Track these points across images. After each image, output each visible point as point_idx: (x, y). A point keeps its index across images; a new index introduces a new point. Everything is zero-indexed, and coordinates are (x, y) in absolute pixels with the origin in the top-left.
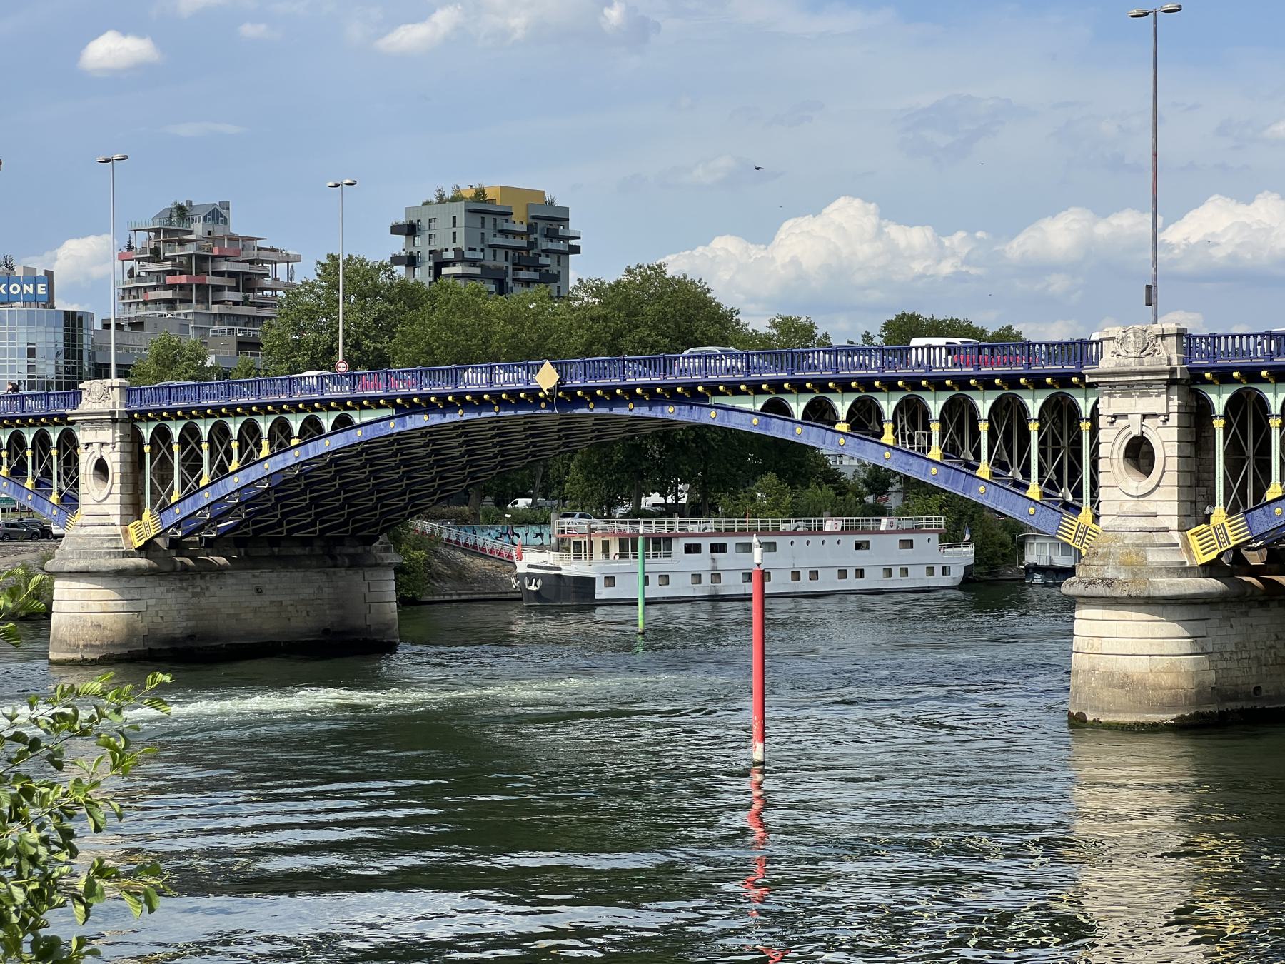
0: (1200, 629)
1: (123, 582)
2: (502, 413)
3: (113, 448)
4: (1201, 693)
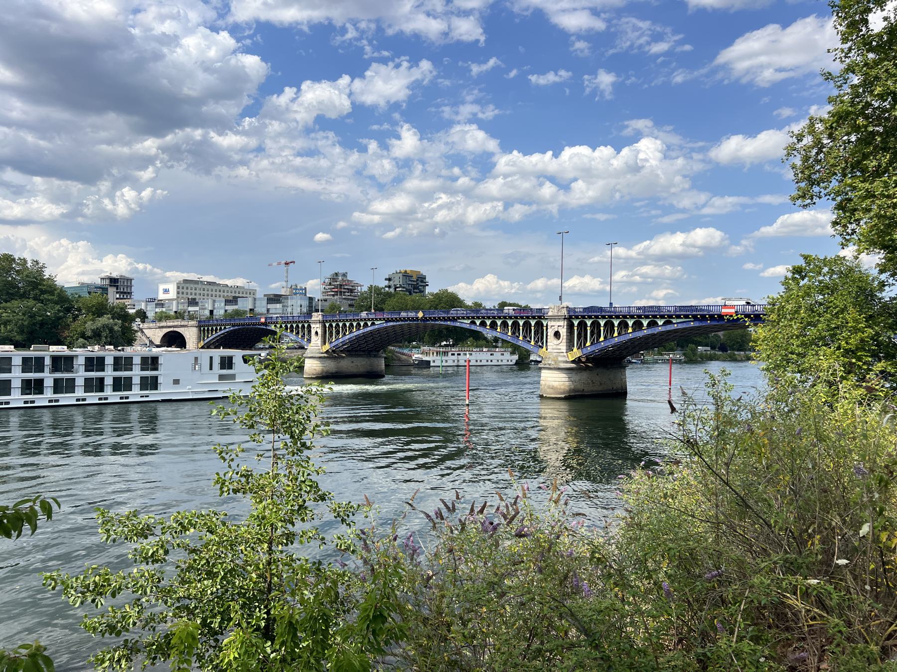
0: (570, 376)
4: (570, 391)
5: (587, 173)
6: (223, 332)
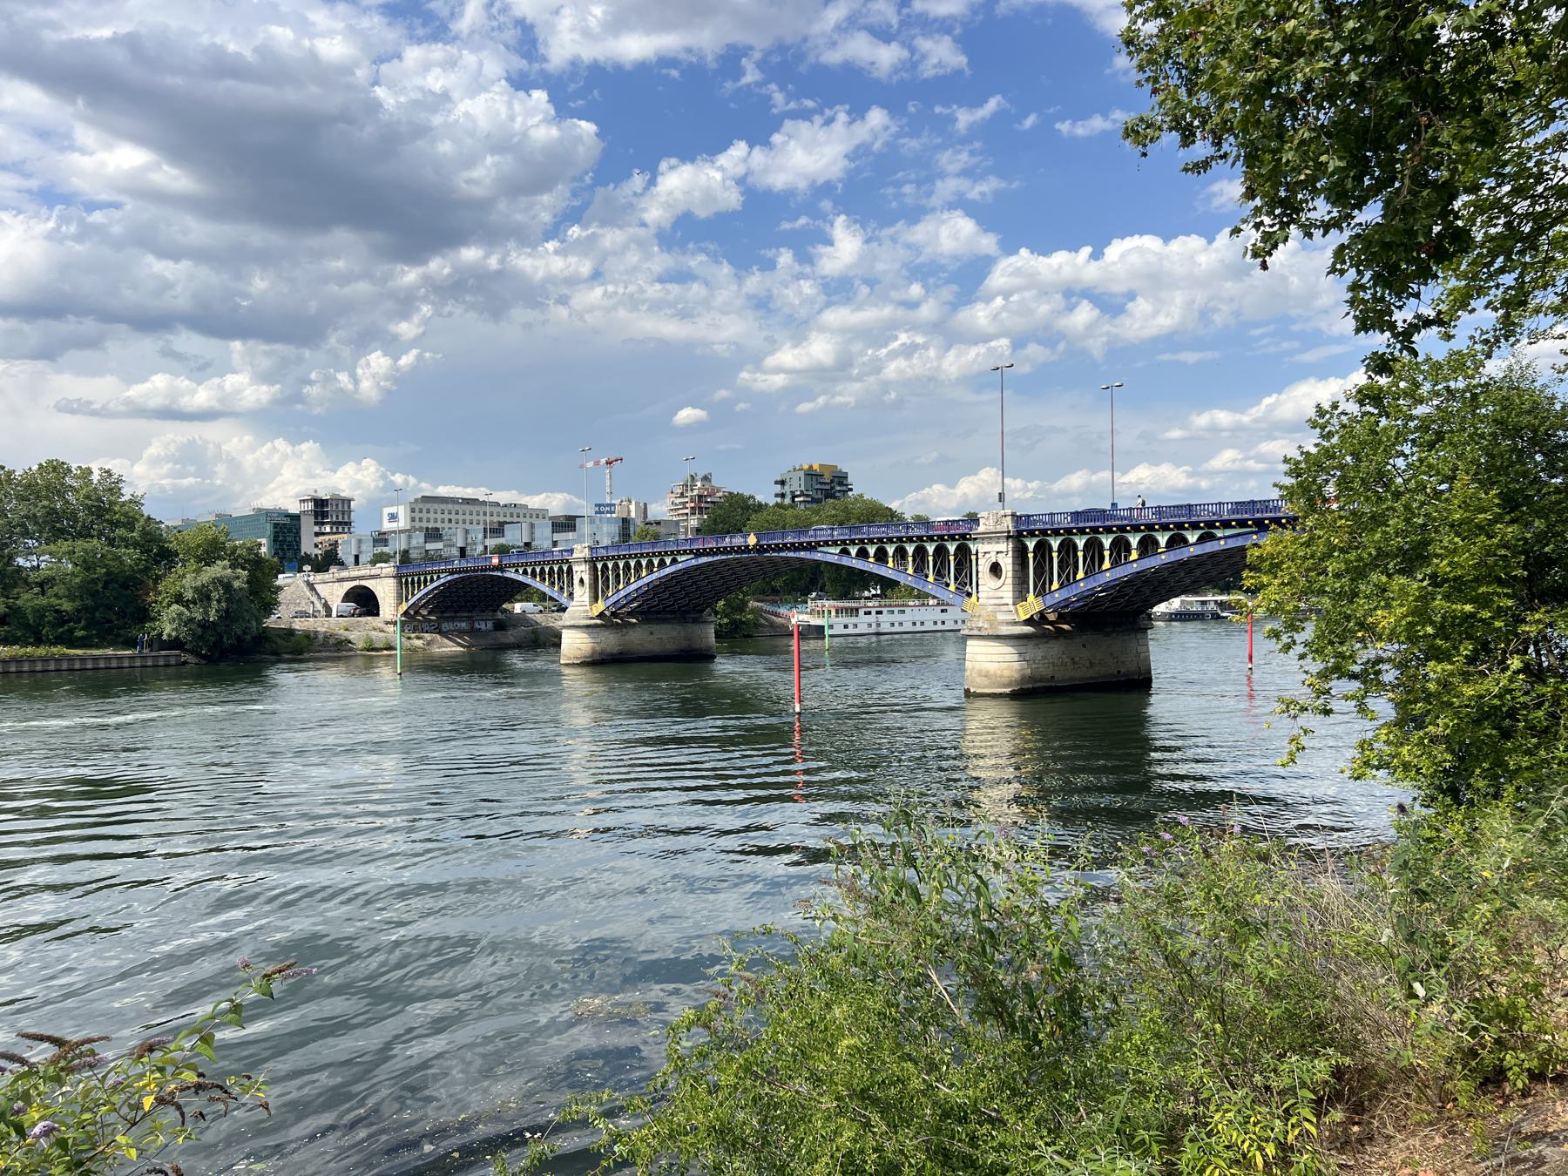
0: (1023, 649)
4: (1023, 679)
5: (1156, 281)
6: (435, 584)
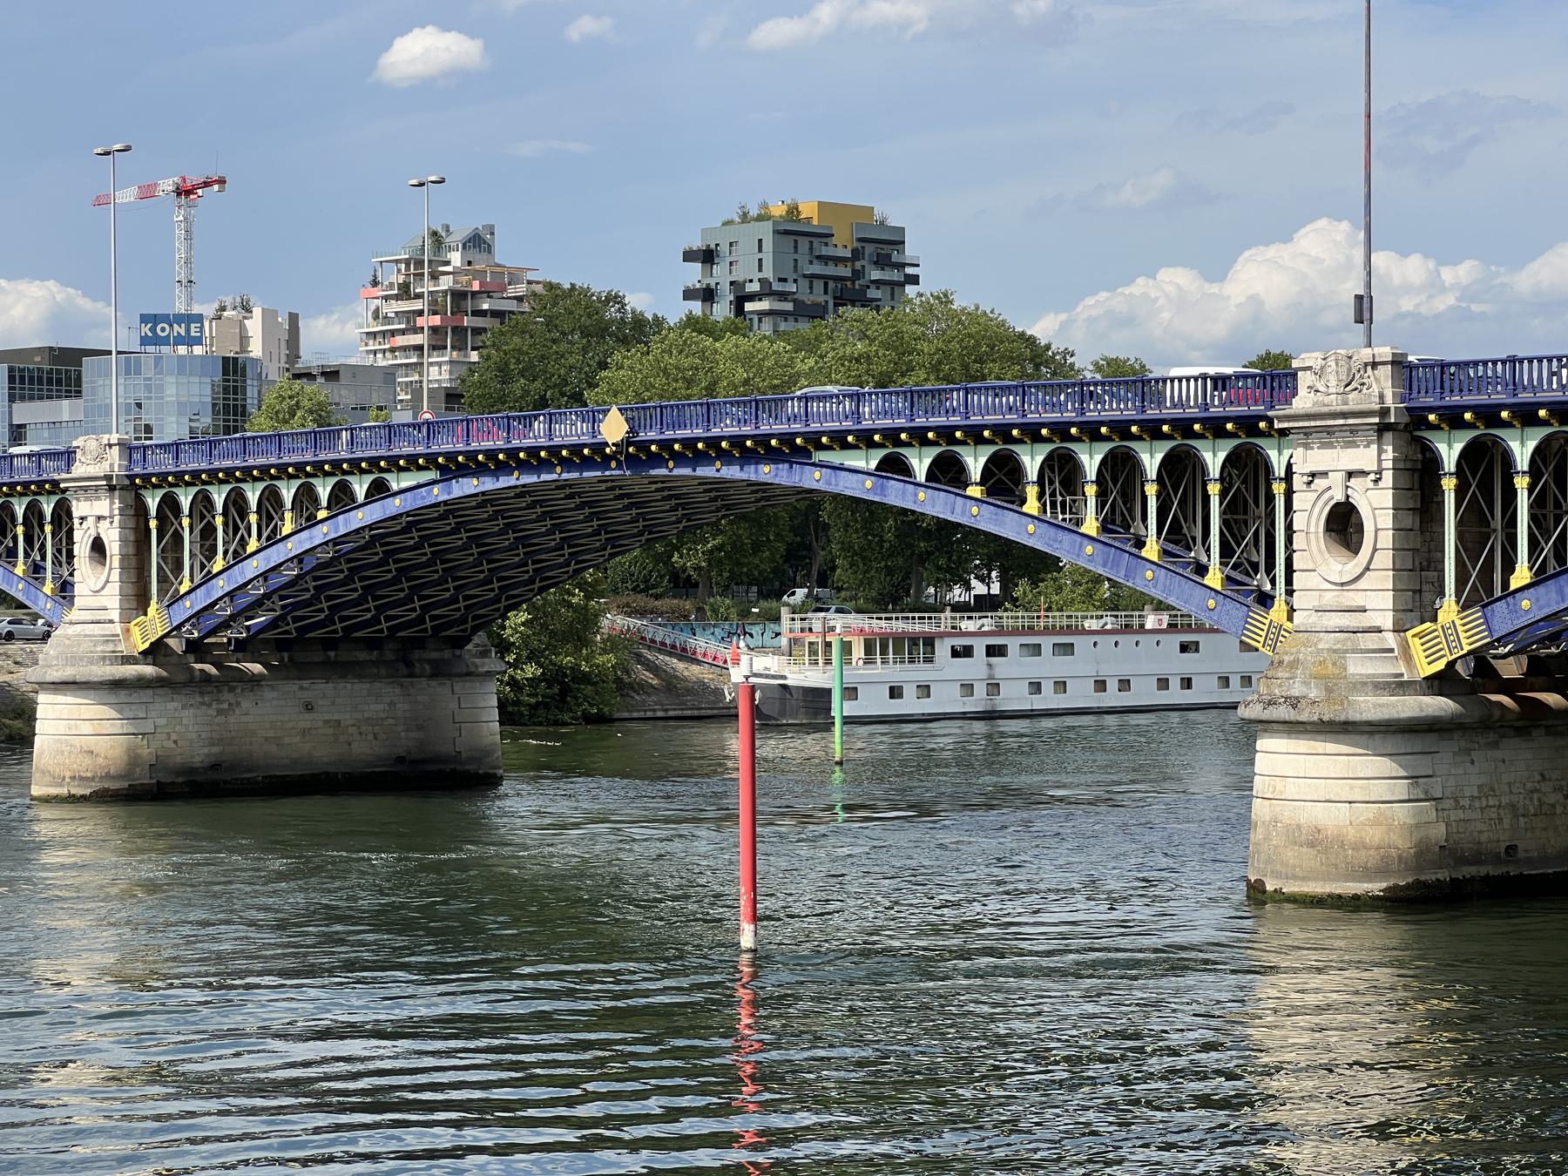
0: (1423, 765)
1: (123, 695)
2: (565, 476)
3: (112, 523)
4: (1423, 854)
